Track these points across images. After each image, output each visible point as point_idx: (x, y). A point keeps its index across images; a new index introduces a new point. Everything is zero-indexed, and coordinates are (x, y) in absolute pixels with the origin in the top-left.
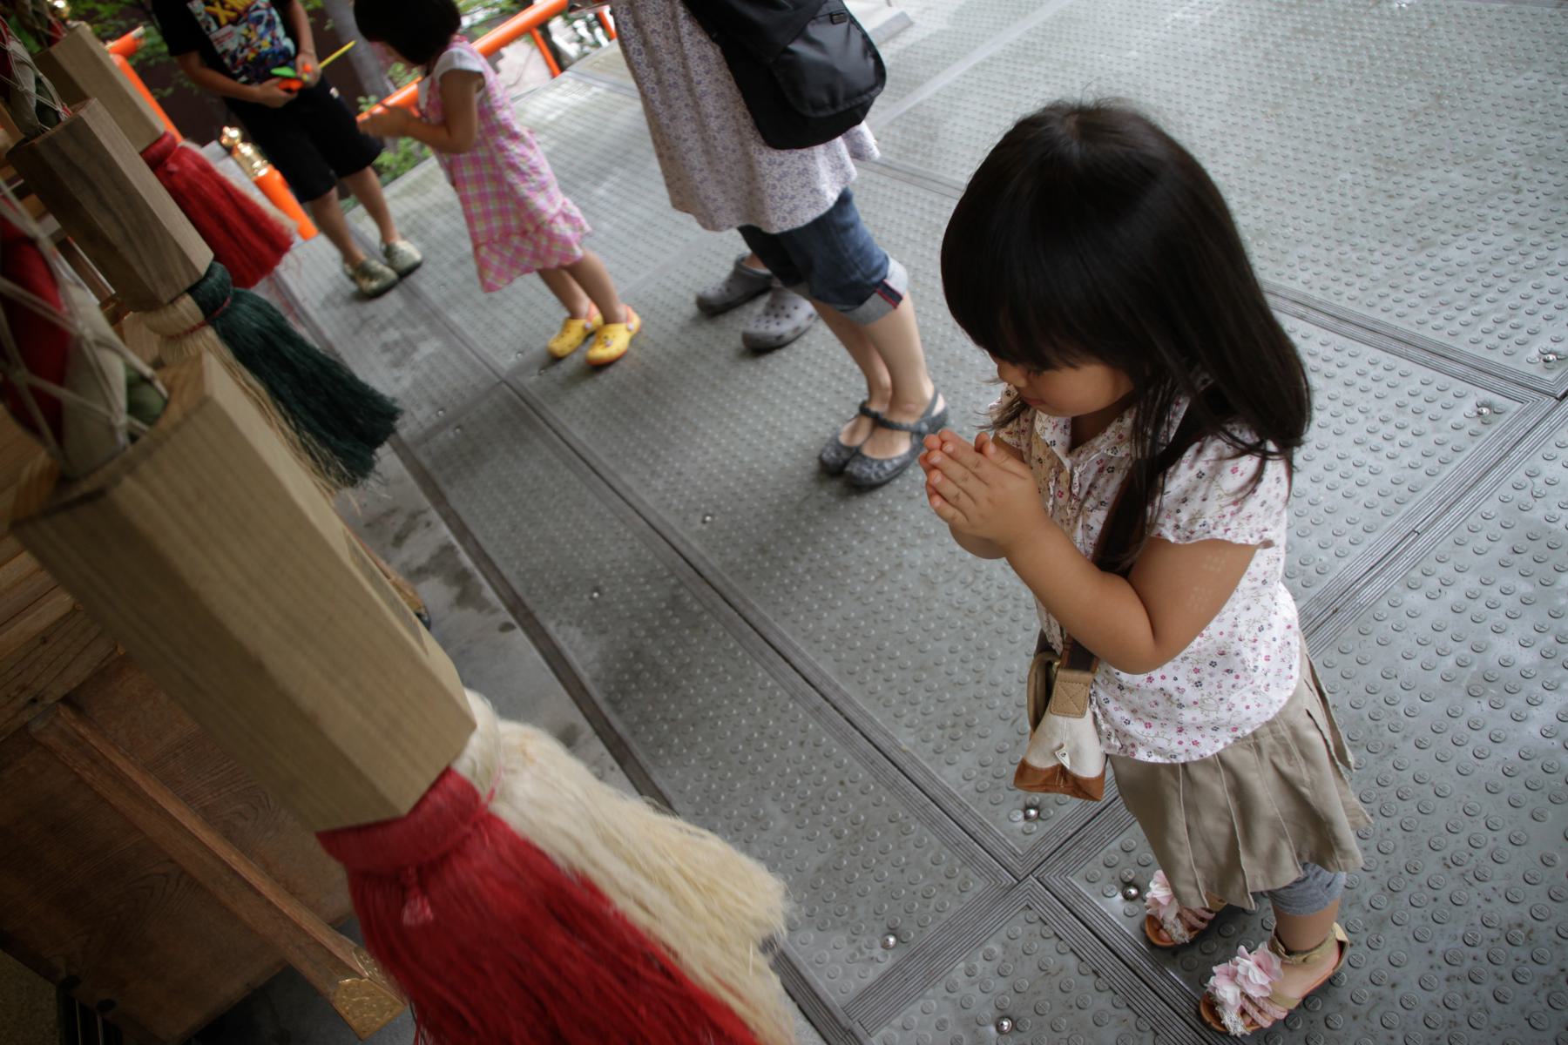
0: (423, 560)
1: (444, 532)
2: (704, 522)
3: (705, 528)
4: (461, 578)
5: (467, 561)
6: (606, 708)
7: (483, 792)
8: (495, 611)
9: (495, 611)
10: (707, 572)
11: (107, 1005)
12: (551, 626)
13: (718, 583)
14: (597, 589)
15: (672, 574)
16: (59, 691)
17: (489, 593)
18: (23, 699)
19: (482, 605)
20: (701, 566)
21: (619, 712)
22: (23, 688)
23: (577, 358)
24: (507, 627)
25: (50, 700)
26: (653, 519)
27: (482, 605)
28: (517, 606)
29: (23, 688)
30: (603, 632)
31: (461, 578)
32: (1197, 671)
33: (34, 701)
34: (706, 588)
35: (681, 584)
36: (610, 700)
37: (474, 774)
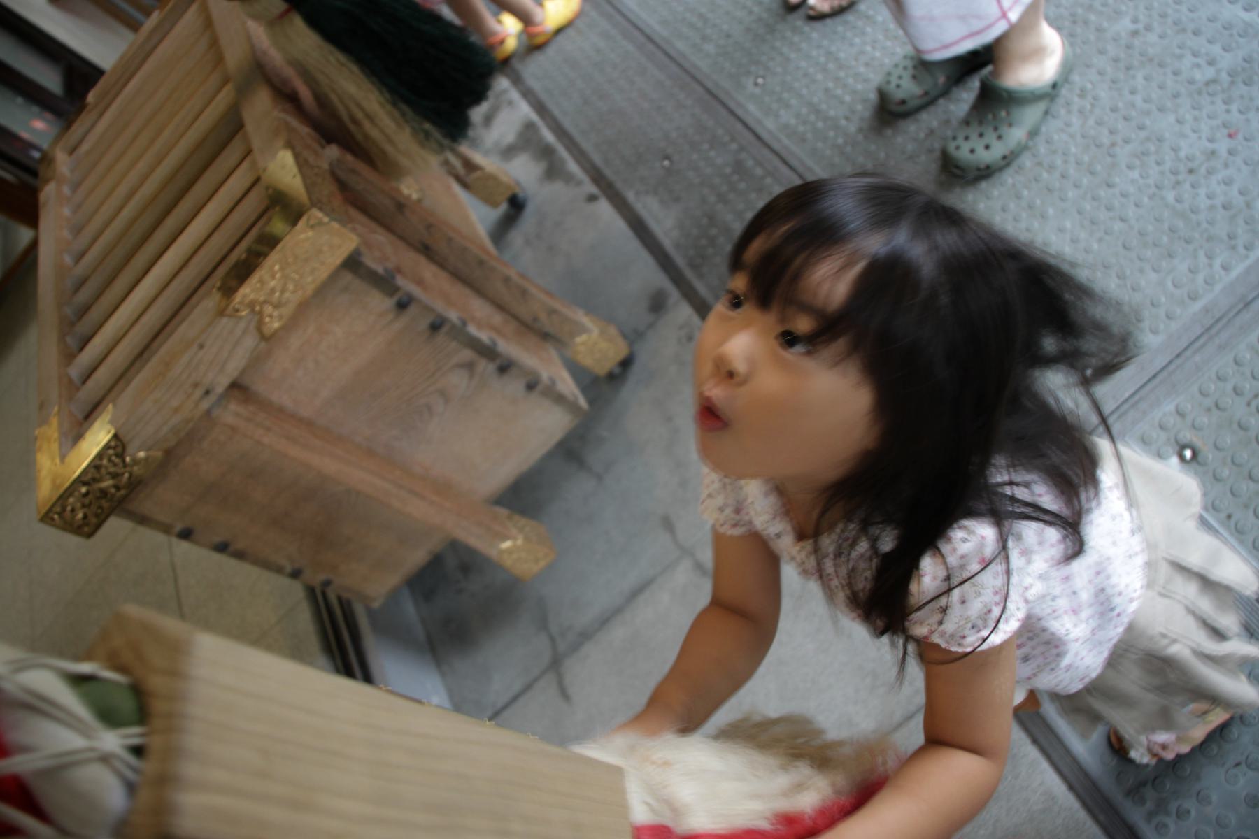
0: (510, 138)
1: (524, 110)
2: (756, 84)
3: (758, 91)
4: (546, 153)
5: (549, 136)
6: (689, 274)
7: (667, 820)
8: (579, 183)
9: (579, 183)
10: (765, 136)
11: (327, 583)
12: (630, 196)
13: (776, 146)
14: (667, 157)
15: (733, 139)
16: (223, 382)
17: (573, 166)
18: (199, 392)
19: (569, 179)
20: (759, 130)
21: (701, 276)
22: (196, 385)
23: (846, 552)
24: (592, 198)
25: (220, 389)
26: (710, 85)
27: (569, 179)
28: (597, 177)
29: (196, 385)
30: (677, 200)
31: (546, 153)
32: (1211, 140)
33: (207, 393)
34: (766, 152)
35: (742, 149)
36: (693, 266)
37: (653, 810)
